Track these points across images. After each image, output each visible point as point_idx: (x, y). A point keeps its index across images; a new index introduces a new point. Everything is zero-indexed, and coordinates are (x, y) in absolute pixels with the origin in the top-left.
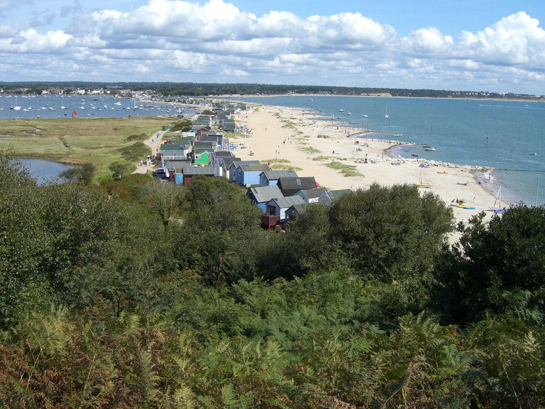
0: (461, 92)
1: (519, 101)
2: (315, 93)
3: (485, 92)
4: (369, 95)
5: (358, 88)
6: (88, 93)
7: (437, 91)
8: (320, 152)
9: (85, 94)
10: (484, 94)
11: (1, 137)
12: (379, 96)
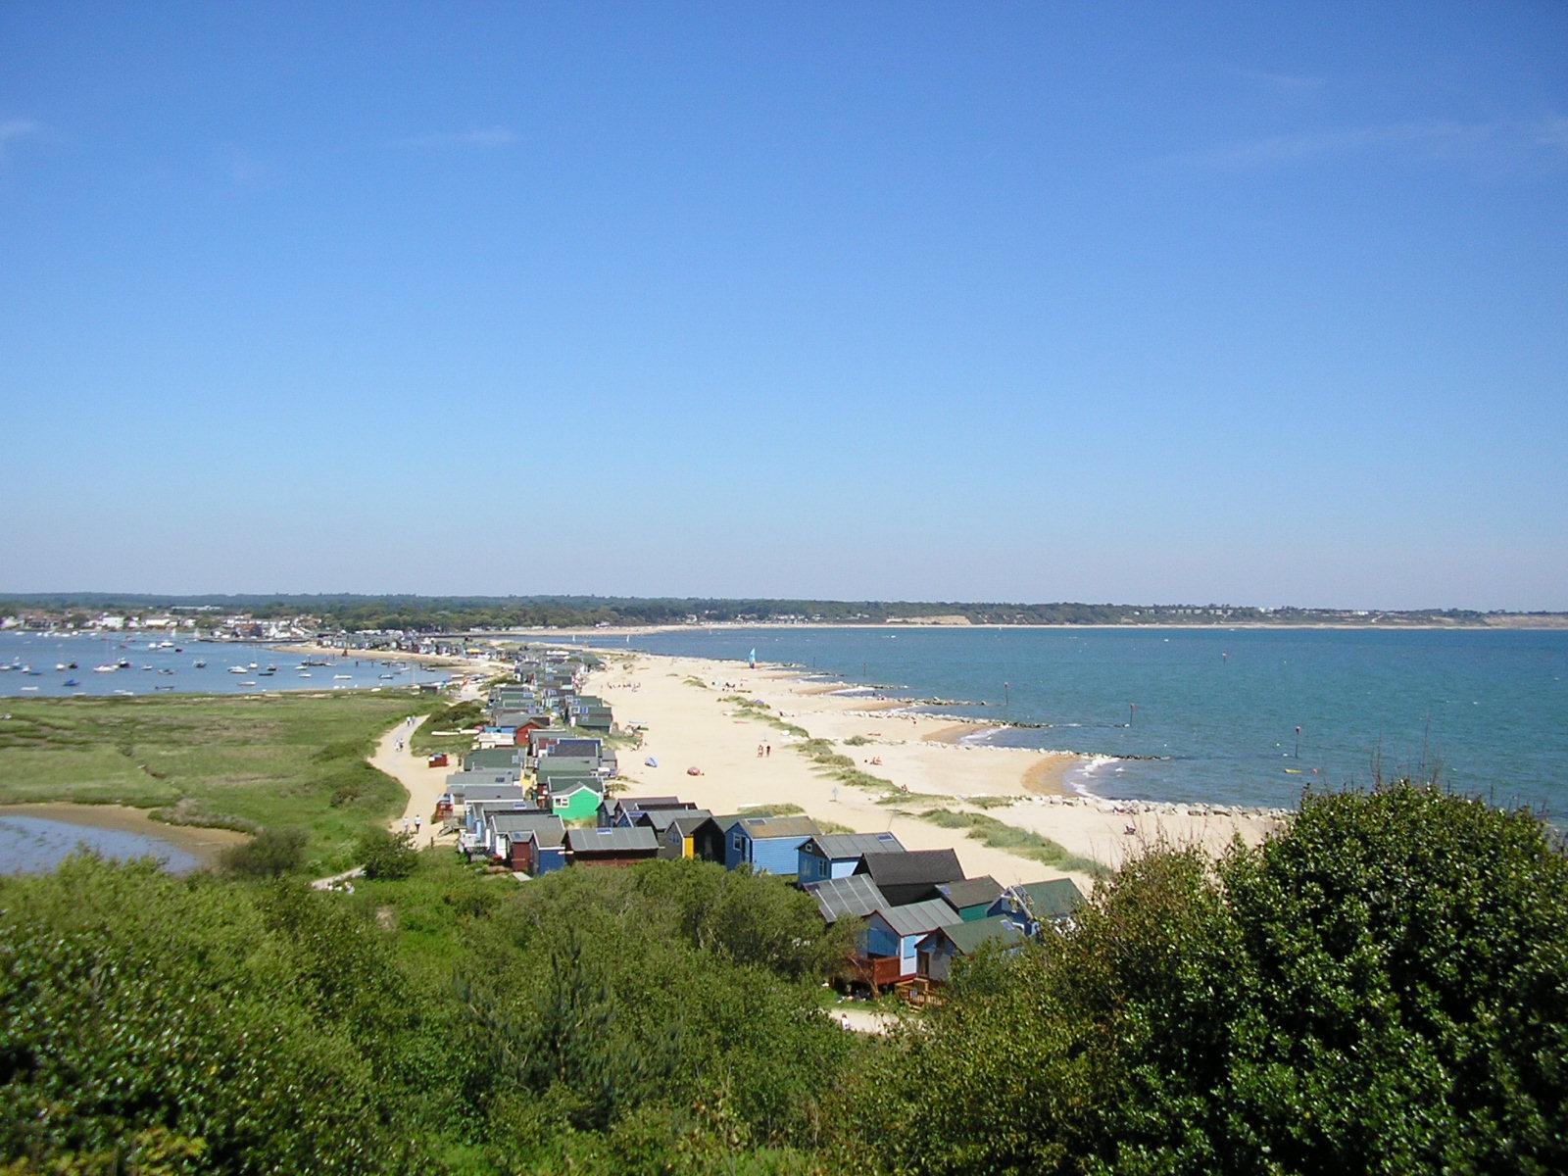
0: (1156, 607)
1: (1317, 627)
2: (761, 618)
3: (1220, 606)
4: (907, 623)
5: (876, 604)
6: (133, 624)
7: (1092, 607)
8: (802, 810)
9: (125, 627)
10: (1219, 612)
11: (2, 739)
12: (935, 623)
